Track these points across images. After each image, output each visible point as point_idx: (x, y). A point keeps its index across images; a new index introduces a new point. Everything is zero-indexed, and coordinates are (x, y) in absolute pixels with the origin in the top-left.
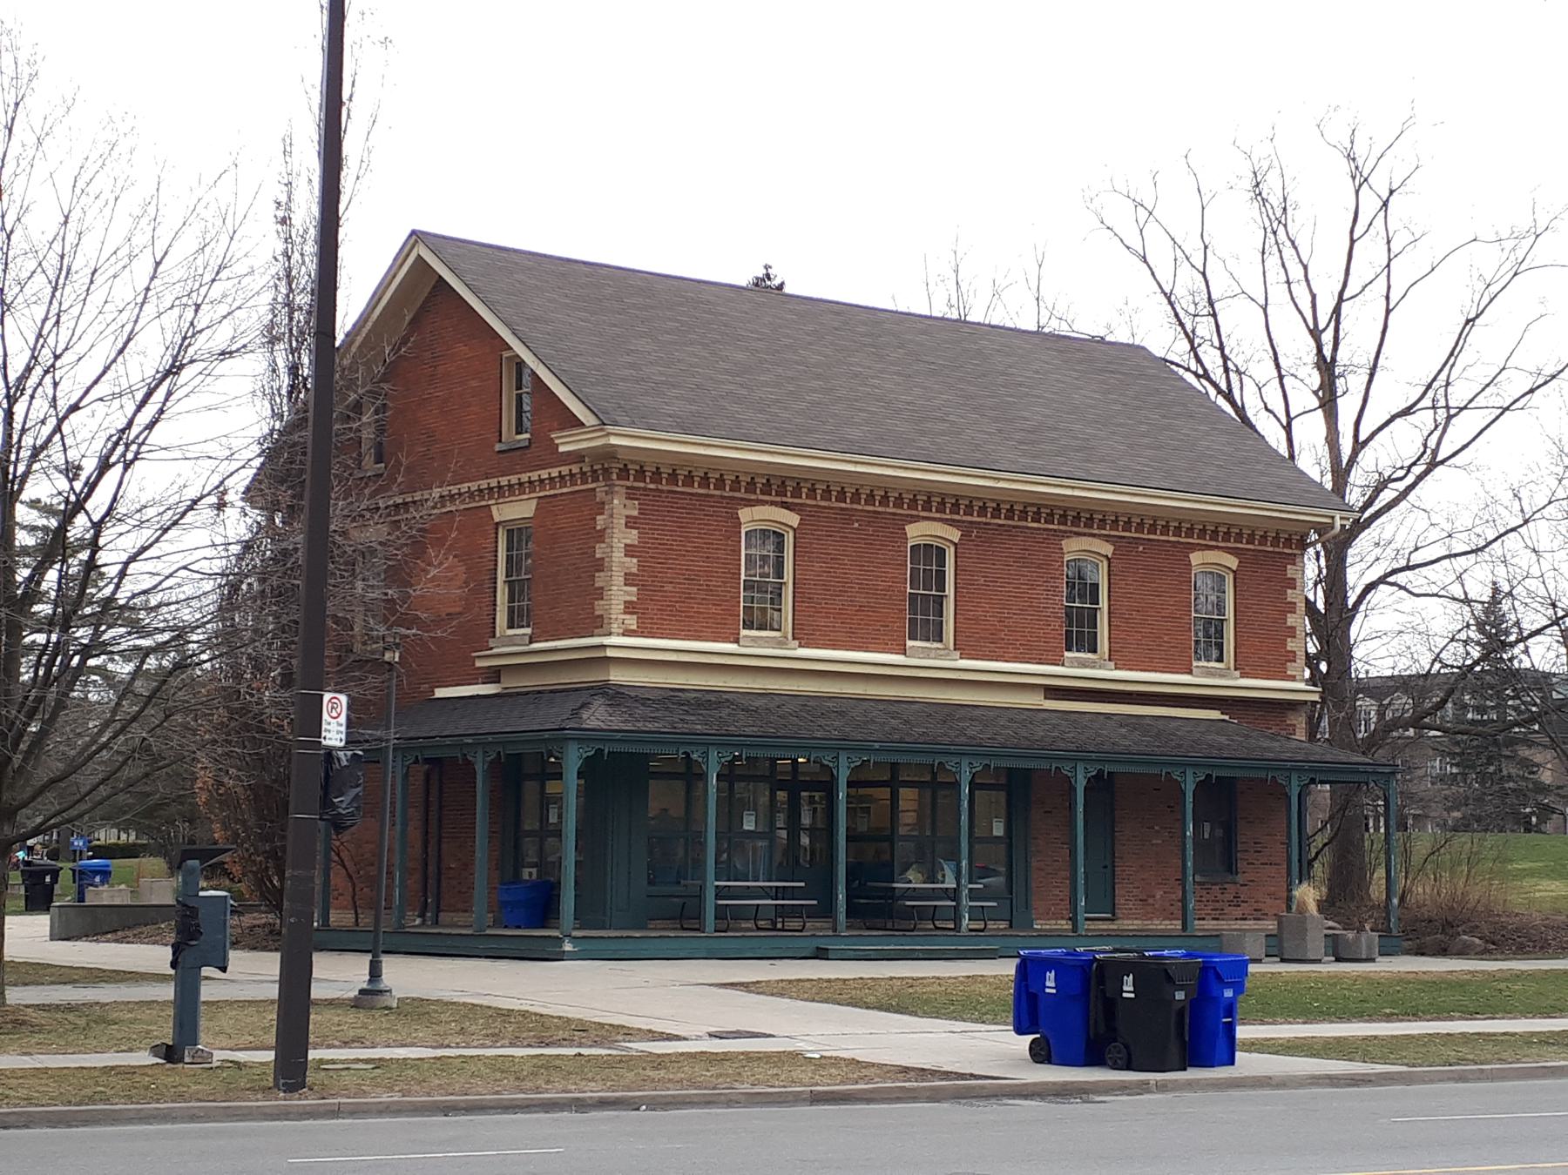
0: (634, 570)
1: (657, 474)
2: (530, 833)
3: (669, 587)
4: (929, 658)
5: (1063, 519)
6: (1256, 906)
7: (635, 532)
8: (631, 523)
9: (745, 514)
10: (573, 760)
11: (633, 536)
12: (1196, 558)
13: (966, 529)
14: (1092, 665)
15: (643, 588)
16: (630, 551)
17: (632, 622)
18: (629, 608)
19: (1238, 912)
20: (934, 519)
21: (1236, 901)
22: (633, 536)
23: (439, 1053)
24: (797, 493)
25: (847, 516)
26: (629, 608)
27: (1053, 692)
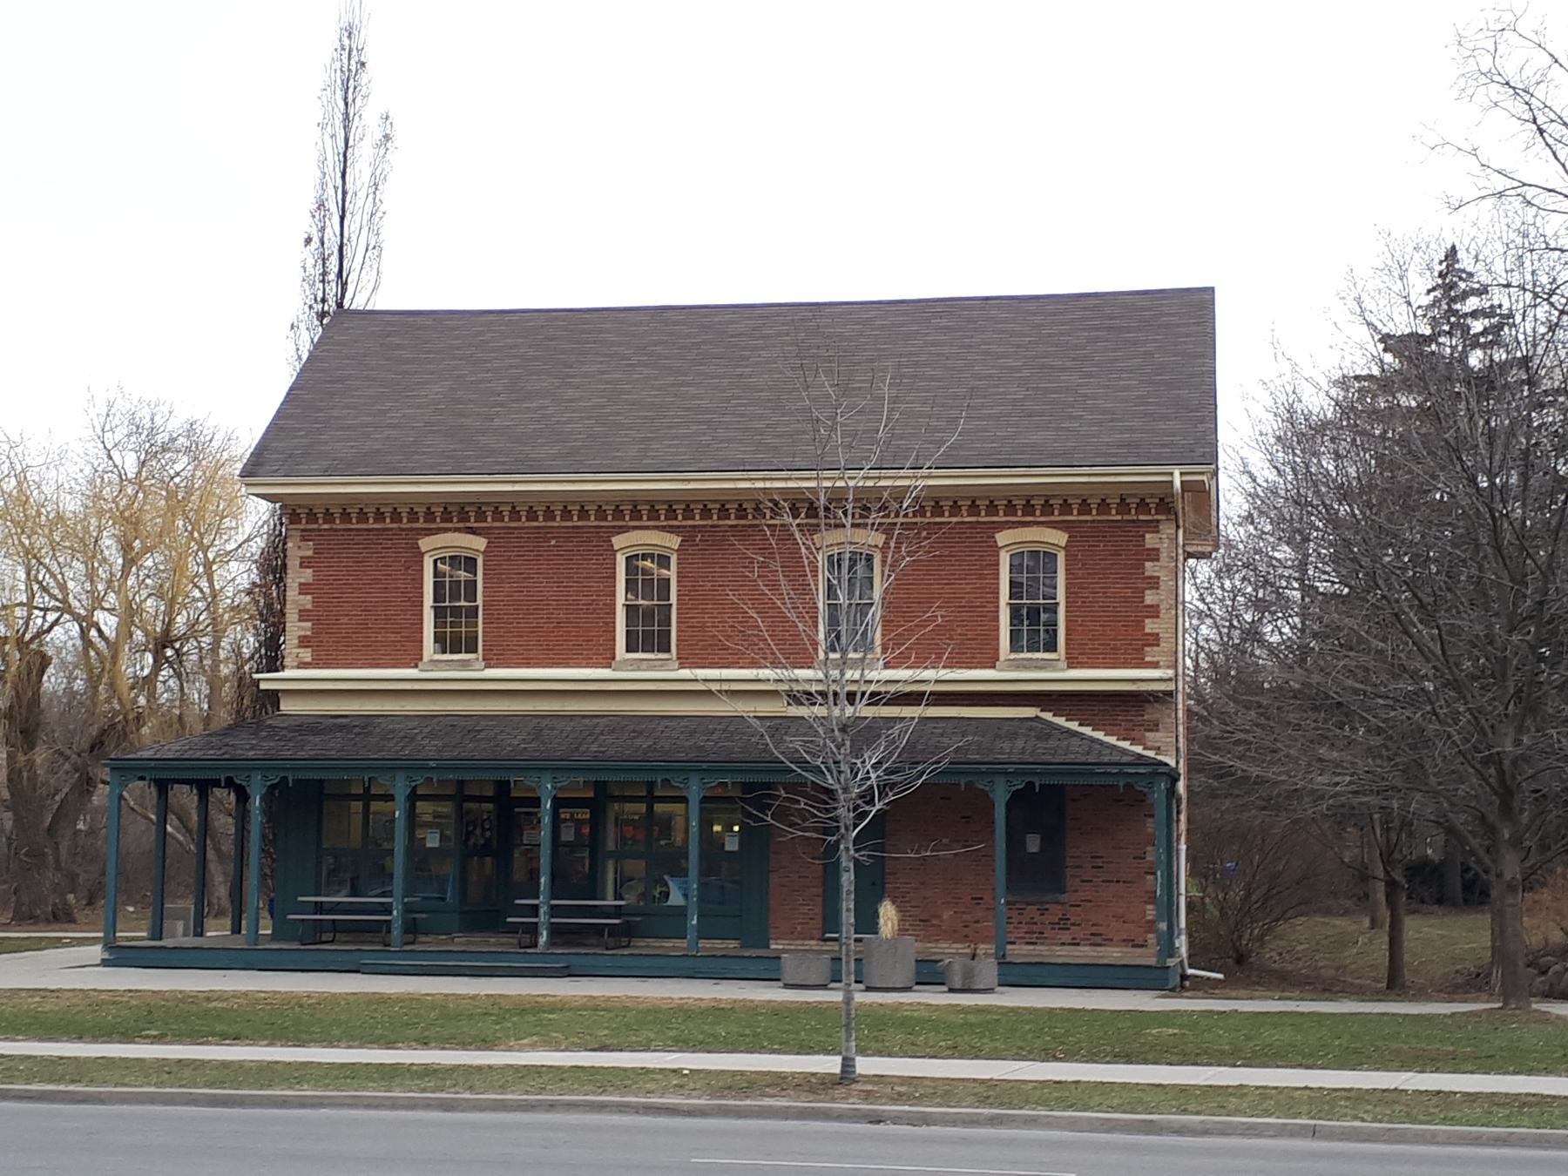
0: (309, 607)
1: (1104, 506)
2: (611, 855)
3: (345, 620)
4: (639, 669)
5: (1010, 508)
6: (1094, 929)
7: (309, 571)
8: (305, 563)
9: (425, 543)
10: (1000, 796)
11: (307, 575)
12: (618, 541)
13: (688, 536)
14: (465, 665)
15: (317, 622)
16: (304, 589)
17: (307, 655)
18: (304, 642)
19: (1066, 936)
20: (647, 528)
21: (1063, 924)
22: (307, 575)
23: (1312, 1122)
24: (481, 516)
25: (542, 535)
26: (304, 642)
27: (794, 698)
